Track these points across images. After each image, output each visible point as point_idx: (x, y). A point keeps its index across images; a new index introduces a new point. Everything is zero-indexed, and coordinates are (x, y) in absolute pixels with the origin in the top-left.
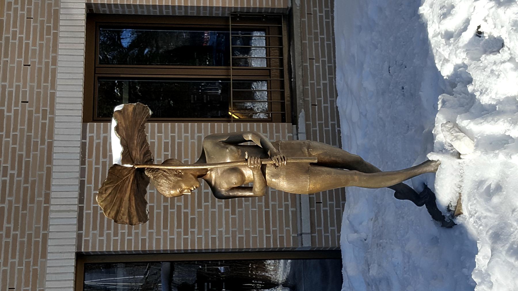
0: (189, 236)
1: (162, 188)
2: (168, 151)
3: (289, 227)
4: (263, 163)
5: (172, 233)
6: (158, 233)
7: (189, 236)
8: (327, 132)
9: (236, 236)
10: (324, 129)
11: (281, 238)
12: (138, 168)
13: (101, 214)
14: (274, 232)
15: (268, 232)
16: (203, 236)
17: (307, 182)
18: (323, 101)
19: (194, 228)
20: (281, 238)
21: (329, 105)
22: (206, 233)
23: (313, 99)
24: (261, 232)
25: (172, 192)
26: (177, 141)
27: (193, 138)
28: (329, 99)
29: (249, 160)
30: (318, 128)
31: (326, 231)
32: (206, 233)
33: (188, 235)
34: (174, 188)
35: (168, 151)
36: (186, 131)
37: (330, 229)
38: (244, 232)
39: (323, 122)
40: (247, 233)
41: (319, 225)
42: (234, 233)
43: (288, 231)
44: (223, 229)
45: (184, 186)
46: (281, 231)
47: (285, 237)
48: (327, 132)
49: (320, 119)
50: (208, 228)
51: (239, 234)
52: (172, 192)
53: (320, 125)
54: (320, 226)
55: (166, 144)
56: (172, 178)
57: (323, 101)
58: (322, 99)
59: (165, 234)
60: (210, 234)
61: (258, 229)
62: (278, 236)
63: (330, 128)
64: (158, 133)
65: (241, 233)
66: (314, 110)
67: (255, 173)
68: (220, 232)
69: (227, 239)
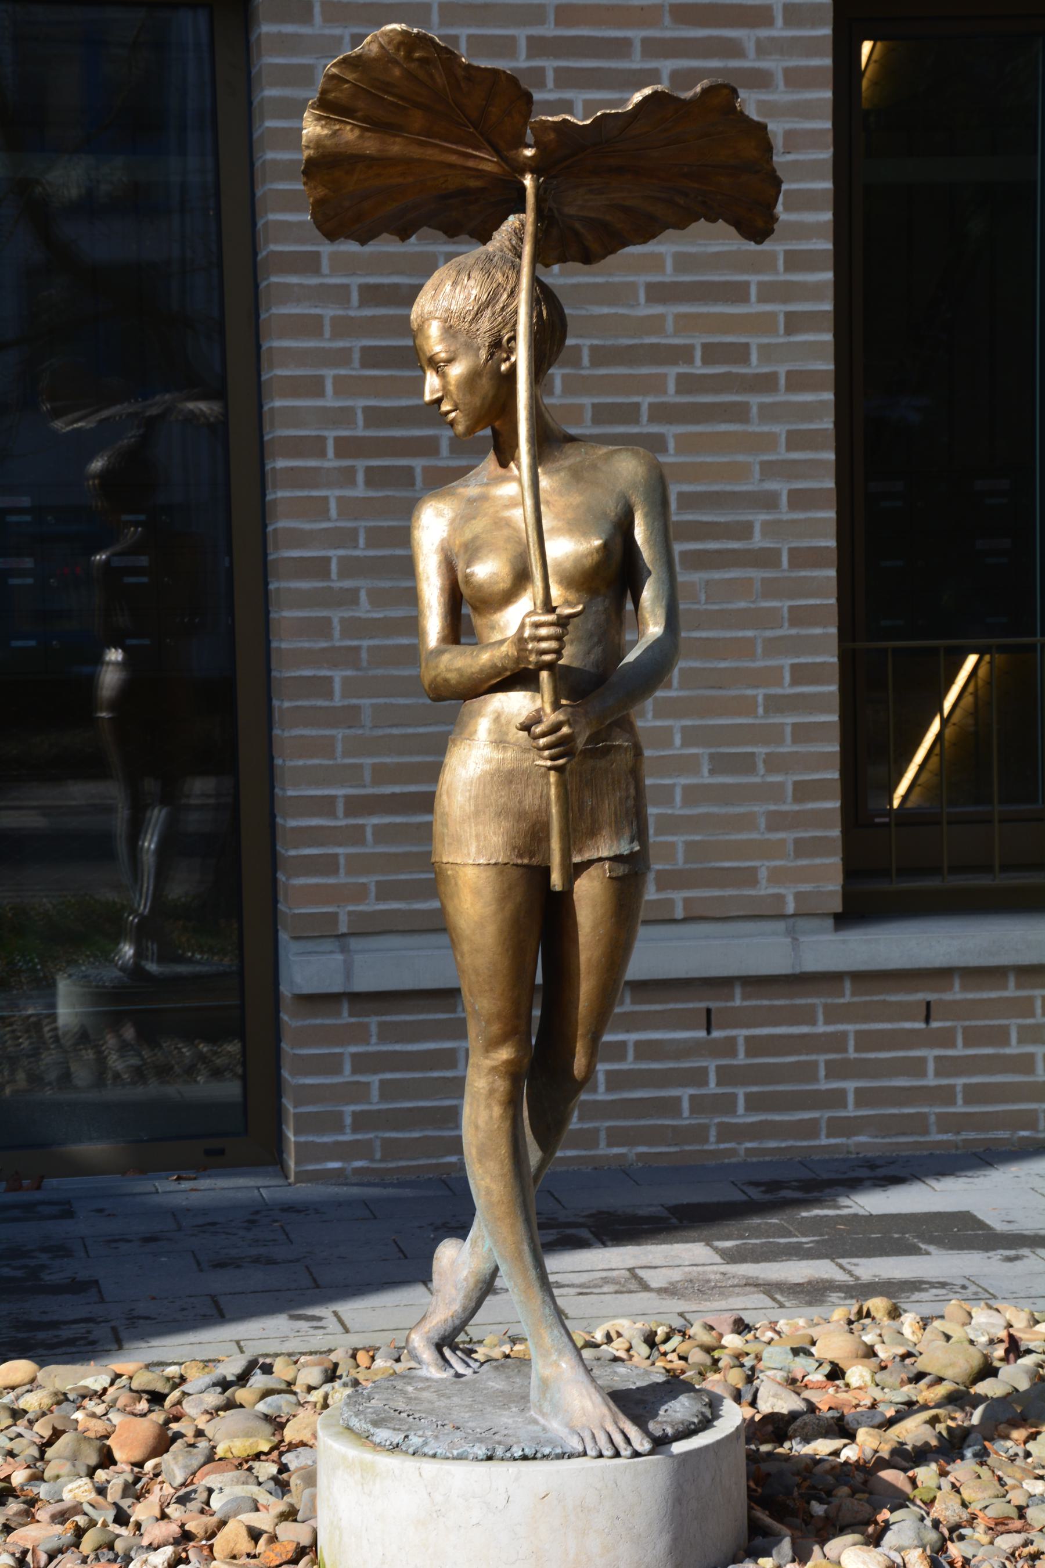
0: (331, 462)
1: (448, 287)
2: (705, 361)
3: (379, 898)
4: (544, 675)
5: (343, 386)
6: (344, 327)
7: (331, 462)
8: (808, 1072)
9: (335, 665)
10: (822, 1058)
11: (329, 865)
12: (524, 188)
13: (336, 42)
14: (356, 836)
15: (358, 806)
16: (334, 521)
17: (479, 852)
18: (950, 1052)
19: (369, 483)
20: (329, 865)
21: (931, 1081)
22: (348, 538)
23: (954, 1010)
24: (352, 774)
25: (434, 329)
26: (755, 400)
27: (770, 470)
28: (960, 1081)
29: (551, 618)
30: (821, 1028)
31: (362, 1064)
32: (348, 538)
33: (338, 455)
34: (449, 332)
35: (705, 361)
36: (795, 440)
37: (374, 1079)
38: (354, 701)
39: (852, 1054)
40: (349, 716)
41: (387, 1033)
42: (349, 657)
43: (360, 893)
44: (364, 610)
45: (456, 371)
46: (358, 865)
47: (331, 880)
48: (808, 1072)
49: (865, 1041)
50: (967, 1102)
51: (345, 680)
52: (434, 329)
53: (837, 1042)
54: (383, 1039)
55: (740, 353)
56: (485, 324)
57: (950, 1052)
58: (959, 1051)
59: (342, 357)
60: (341, 552)
61: (369, 761)
62: (340, 850)
63: (824, 1085)
64: (788, 315)
65: (351, 687)
66: (904, 1012)
67: (504, 648)
68: (351, 598)
69: (323, 628)
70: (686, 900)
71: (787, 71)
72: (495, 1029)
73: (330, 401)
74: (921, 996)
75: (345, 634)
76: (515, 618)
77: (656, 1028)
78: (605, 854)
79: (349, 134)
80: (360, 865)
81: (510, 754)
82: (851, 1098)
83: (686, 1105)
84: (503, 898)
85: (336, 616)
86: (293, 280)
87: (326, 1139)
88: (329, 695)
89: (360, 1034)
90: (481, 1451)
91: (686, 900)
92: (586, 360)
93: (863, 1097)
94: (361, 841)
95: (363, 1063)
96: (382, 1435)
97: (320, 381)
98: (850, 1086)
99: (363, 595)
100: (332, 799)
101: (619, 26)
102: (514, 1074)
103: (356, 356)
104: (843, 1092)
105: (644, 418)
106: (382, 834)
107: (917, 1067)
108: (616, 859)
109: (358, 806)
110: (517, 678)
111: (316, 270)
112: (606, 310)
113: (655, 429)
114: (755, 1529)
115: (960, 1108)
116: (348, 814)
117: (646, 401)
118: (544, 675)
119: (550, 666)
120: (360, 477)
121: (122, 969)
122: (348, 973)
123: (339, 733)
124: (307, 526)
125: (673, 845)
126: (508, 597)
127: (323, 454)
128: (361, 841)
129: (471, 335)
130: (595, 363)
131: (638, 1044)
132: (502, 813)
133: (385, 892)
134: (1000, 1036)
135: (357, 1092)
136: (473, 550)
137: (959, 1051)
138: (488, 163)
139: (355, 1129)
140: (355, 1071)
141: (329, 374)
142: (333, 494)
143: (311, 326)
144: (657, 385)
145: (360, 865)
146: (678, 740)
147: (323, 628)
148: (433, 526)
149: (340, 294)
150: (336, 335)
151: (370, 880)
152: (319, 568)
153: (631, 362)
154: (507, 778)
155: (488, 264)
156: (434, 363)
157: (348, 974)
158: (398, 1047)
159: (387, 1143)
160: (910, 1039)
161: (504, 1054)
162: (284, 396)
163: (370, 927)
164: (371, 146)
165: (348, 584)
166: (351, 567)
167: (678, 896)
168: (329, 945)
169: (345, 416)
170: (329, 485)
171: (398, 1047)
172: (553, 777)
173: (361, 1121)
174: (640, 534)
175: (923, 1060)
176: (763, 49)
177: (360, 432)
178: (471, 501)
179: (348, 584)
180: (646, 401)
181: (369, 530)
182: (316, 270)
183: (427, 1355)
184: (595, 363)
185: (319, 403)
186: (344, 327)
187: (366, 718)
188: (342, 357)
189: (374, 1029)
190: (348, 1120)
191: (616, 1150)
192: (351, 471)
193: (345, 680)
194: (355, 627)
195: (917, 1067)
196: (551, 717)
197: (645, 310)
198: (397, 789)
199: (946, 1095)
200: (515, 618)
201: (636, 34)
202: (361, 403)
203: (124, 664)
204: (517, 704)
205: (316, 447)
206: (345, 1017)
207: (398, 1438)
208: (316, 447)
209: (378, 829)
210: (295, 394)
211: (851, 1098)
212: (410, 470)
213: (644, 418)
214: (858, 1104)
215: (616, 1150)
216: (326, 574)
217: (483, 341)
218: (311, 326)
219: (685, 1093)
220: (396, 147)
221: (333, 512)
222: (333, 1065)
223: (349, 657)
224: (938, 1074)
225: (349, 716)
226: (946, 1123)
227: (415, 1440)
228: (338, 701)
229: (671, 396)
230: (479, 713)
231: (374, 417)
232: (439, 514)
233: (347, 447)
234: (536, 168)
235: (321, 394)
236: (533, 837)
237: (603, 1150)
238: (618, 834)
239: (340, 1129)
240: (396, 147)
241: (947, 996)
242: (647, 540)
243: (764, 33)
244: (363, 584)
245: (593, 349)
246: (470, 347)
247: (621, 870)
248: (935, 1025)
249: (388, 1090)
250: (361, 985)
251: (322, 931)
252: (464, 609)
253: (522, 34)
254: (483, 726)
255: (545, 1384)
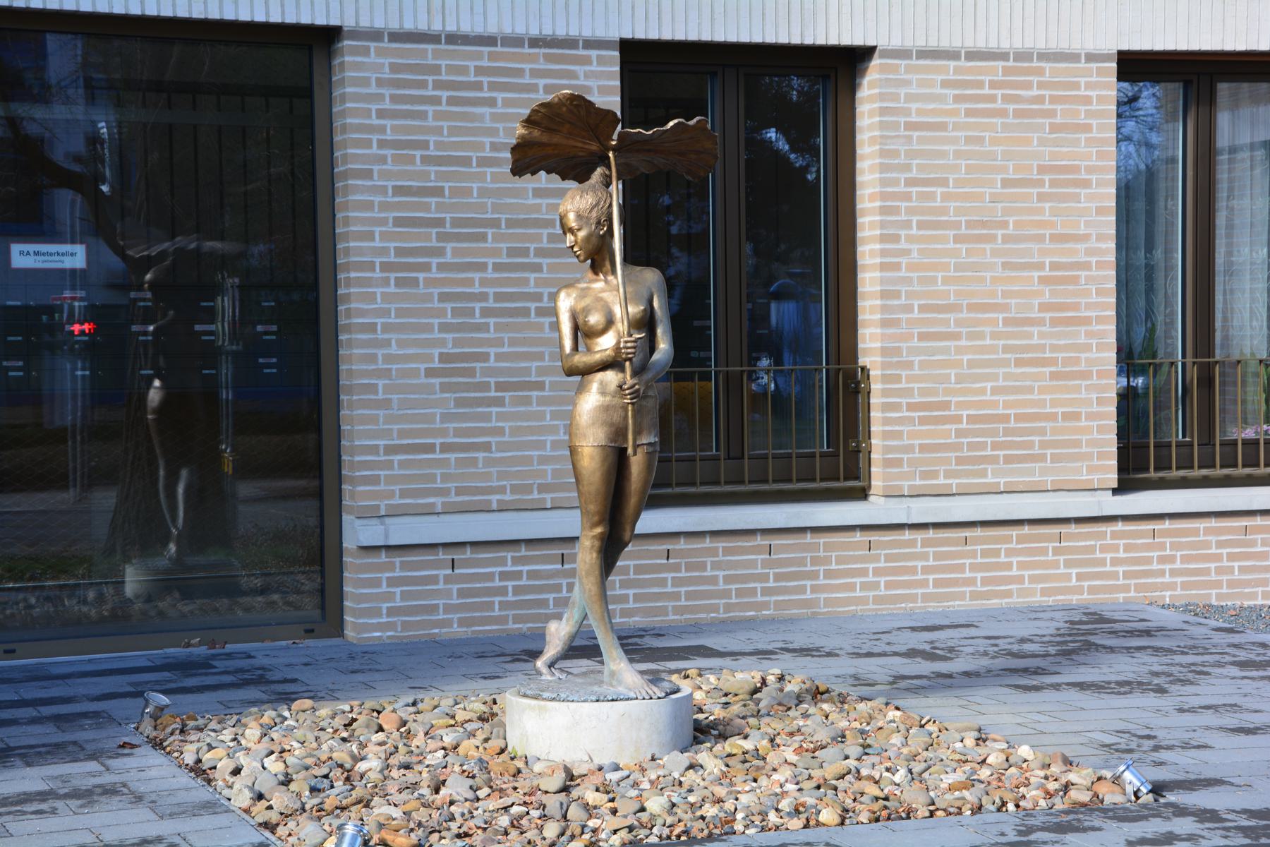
4: (627, 363)
5: (385, 236)
6: (385, 206)
7: (378, 274)
9: (379, 378)
14: (389, 465)
15: (390, 450)
19: (397, 285)
20: (375, 480)
21: (669, 589)
22: (386, 313)
23: (681, 553)
28: (683, 589)
33: (382, 271)
34: (579, 217)
39: (632, 576)
40: (386, 404)
41: (404, 566)
42: (386, 373)
43: (391, 495)
44: (394, 350)
51: (385, 385)
54: (402, 569)
56: (594, 214)
59: (384, 222)
66: (656, 555)
68: (387, 343)
70: (552, 499)
71: (599, 87)
72: (596, 519)
73: (377, 244)
74: (665, 547)
75: (385, 361)
76: (606, 343)
77: (537, 563)
78: (645, 442)
79: (536, 133)
80: (391, 480)
81: (608, 398)
82: (631, 598)
83: (551, 603)
84: (604, 460)
85: (380, 352)
86: (360, 182)
87: (374, 621)
88: (376, 393)
89: (391, 567)
90: (594, 698)
91: (552, 499)
92: (503, 226)
93: (637, 598)
94: (392, 468)
95: (392, 582)
96: (545, 695)
97: (372, 233)
98: (631, 592)
99: (393, 342)
100: (377, 446)
101: (519, 62)
102: (601, 537)
103: (391, 221)
104: (627, 595)
105: (532, 254)
106: (402, 464)
107: (663, 583)
108: (650, 444)
109: (390, 450)
110: (604, 366)
111: (371, 178)
112: (513, 201)
113: (537, 260)
114: (695, 738)
115: (683, 603)
116: (385, 454)
117: (532, 246)
118: (627, 363)
119: (630, 359)
120: (392, 282)
121: (170, 559)
122: (386, 536)
123: (381, 413)
124: (366, 307)
125: (545, 471)
126: (604, 331)
127: (374, 270)
128: (392, 468)
129: (588, 219)
130: (508, 227)
131: (528, 572)
132: (604, 423)
133: (403, 494)
134: (702, 567)
135: (389, 597)
136: (587, 311)
137: (683, 574)
138: (594, 147)
139: (388, 615)
140: (388, 586)
141: (377, 230)
142: (379, 290)
143: (368, 206)
144: (538, 238)
145: (391, 480)
146: (548, 417)
147: (372, 358)
148: (565, 303)
149: (383, 190)
150: (380, 211)
151: (396, 488)
152: (372, 328)
153: (526, 227)
154: (606, 409)
155: (593, 189)
156: (571, 231)
157: (386, 536)
158: (409, 574)
159: (404, 623)
160: (659, 569)
161: (599, 530)
162: (355, 240)
163: (395, 513)
164: (545, 139)
165: (386, 336)
166: (387, 328)
167: (548, 496)
168: (375, 521)
169: (384, 251)
170: (377, 286)
171: (409, 574)
172: (630, 407)
173: (391, 612)
174: (656, 304)
175: (666, 579)
176: (587, 75)
177: (392, 260)
178: (583, 289)
179: (386, 336)
180: (532, 246)
181: (396, 309)
182: (371, 178)
183: (545, 670)
184: (508, 227)
185: (372, 244)
186: (385, 206)
187: (395, 405)
188: (384, 222)
189: (398, 565)
190: (385, 611)
191: (517, 626)
192: (388, 279)
193: (385, 385)
194: (389, 358)
195: (663, 583)
196: (630, 382)
197: (532, 201)
198: (410, 441)
199: (676, 596)
200: (606, 343)
201: (527, 66)
202: (393, 245)
203: (161, 388)
204: (611, 377)
205: (370, 266)
206: (383, 557)
207: (554, 695)
208: (370, 266)
209: (400, 462)
210: (361, 240)
211: (631, 598)
212: (417, 279)
213: (532, 254)
214: (635, 601)
215: (517, 626)
216: (375, 331)
217: (593, 221)
218: (368, 206)
219: (551, 596)
220: (556, 139)
221: (379, 300)
222: (376, 583)
223: (386, 373)
224: (673, 586)
225: (386, 404)
226: (677, 610)
227: (563, 696)
228: (381, 396)
229: (545, 244)
230: (591, 382)
231: (400, 252)
232: (568, 295)
233: (386, 267)
234: (614, 149)
235: (373, 240)
236: (618, 433)
237: (511, 626)
238: (650, 433)
239: (380, 616)
240: (556, 139)
241: (677, 547)
242: (660, 307)
243: (587, 68)
244: (393, 337)
245: (507, 220)
246: (588, 222)
247: (651, 449)
248: (671, 561)
249: (405, 595)
250: (392, 542)
251: (371, 514)
252: (583, 333)
253: (472, 64)
254: (595, 387)
255: (613, 674)
